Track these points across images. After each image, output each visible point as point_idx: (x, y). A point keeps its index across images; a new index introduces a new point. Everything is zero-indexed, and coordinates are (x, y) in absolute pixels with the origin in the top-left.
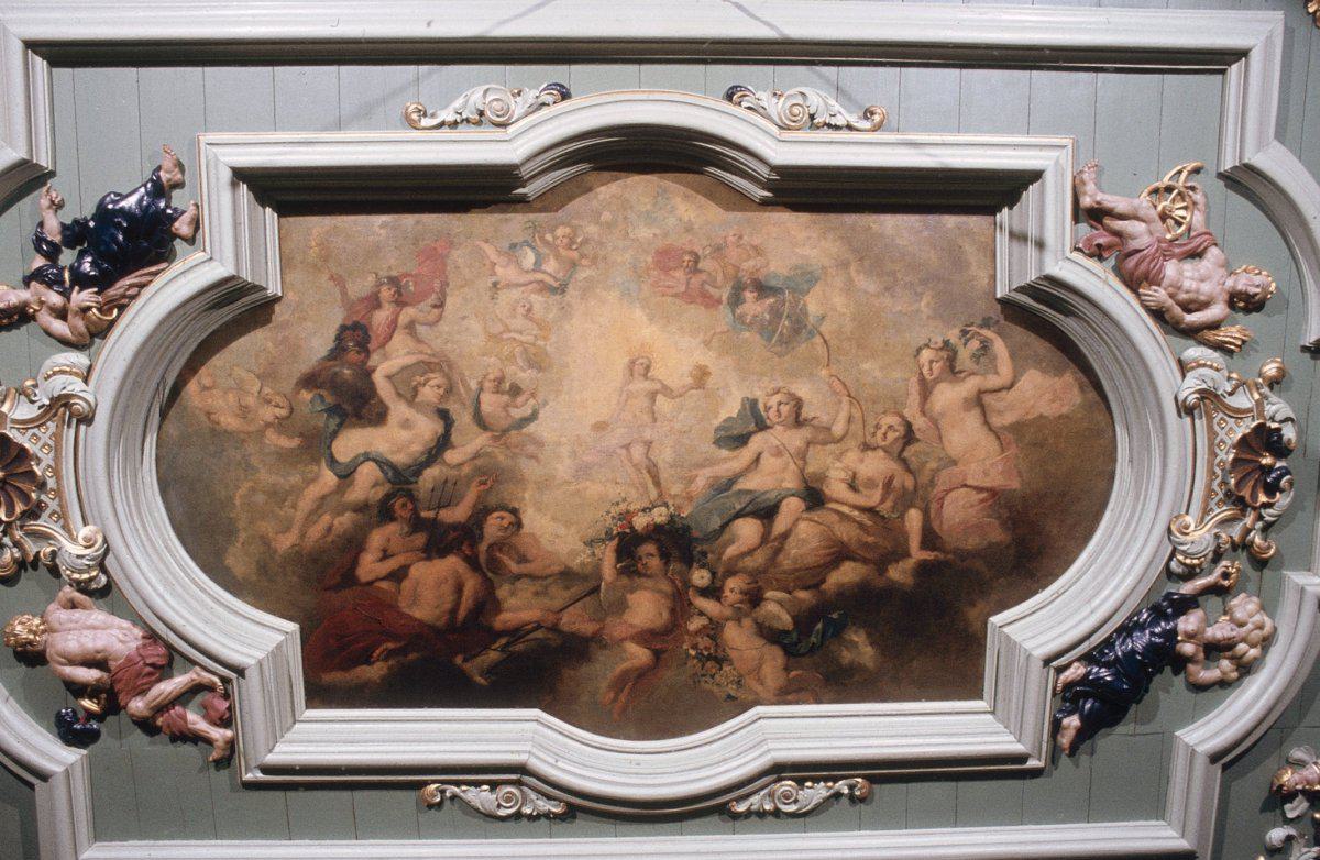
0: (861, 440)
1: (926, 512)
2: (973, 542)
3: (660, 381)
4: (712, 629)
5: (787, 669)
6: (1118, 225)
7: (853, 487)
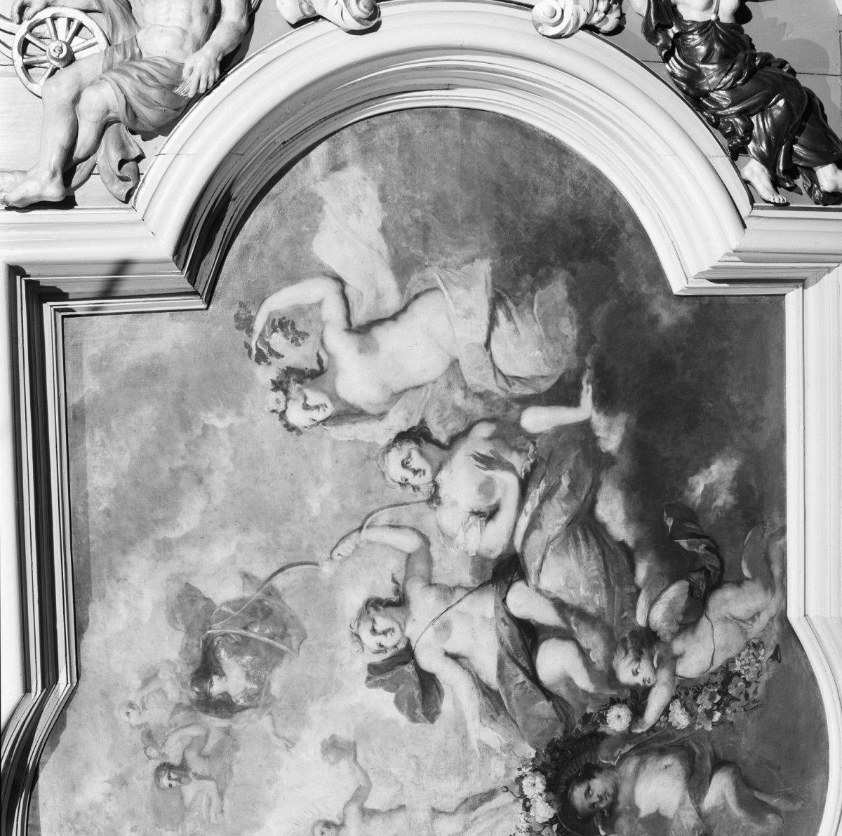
0: (424, 508)
1: (526, 402)
2: (569, 329)
3: (347, 805)
4: (687, 694)
5: (739, 582)
6: (86, 136)
7: (490, 514)
